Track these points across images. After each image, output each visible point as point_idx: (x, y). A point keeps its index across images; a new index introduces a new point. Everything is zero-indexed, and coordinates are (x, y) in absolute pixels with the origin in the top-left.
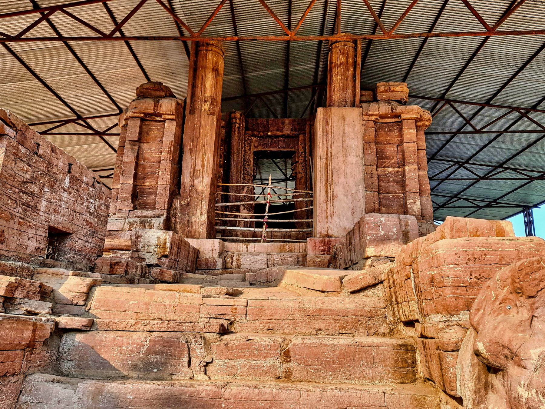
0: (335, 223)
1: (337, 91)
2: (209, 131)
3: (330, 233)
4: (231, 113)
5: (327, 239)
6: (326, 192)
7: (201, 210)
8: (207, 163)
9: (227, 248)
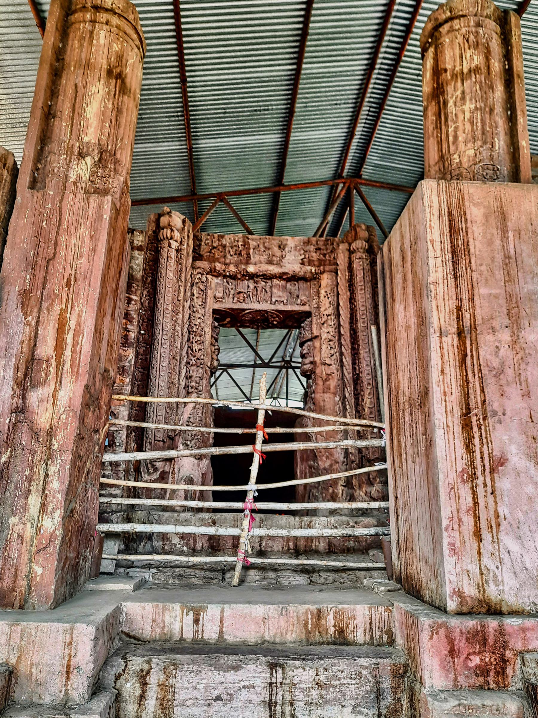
0: (505, 557)
1: (466, 142)
2: (87, 240)
3: (492, 592)
4: (160, 215)
5: (492, 624)
6: (469, 446)
7: (44, 495)
8: (75, 336)
9: (130, 621)
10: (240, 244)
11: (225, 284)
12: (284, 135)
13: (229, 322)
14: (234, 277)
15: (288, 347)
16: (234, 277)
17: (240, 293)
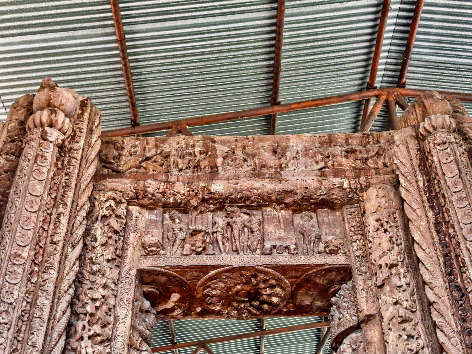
10: (197, 149)
11: (168, 221)
12: (274, 13)
13: (177, 305)
14: (182, 207)
16: (182, 207)
17: (195, 233)
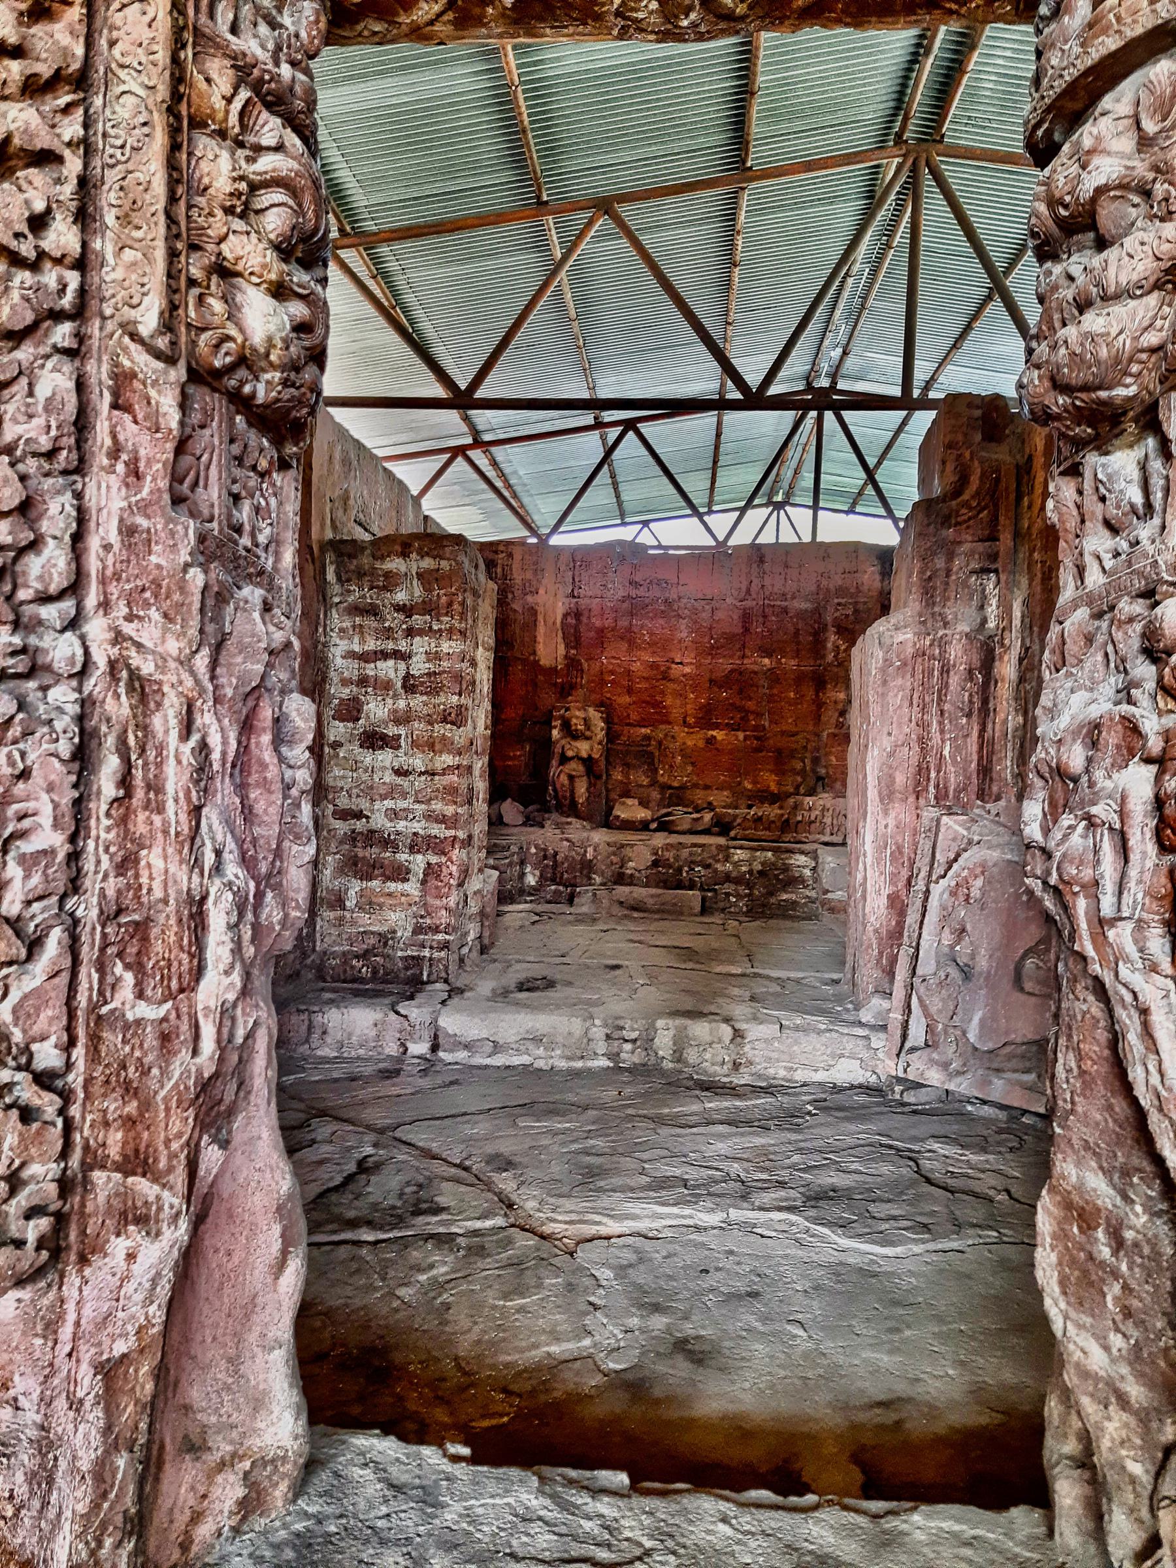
15: (826, 342)
